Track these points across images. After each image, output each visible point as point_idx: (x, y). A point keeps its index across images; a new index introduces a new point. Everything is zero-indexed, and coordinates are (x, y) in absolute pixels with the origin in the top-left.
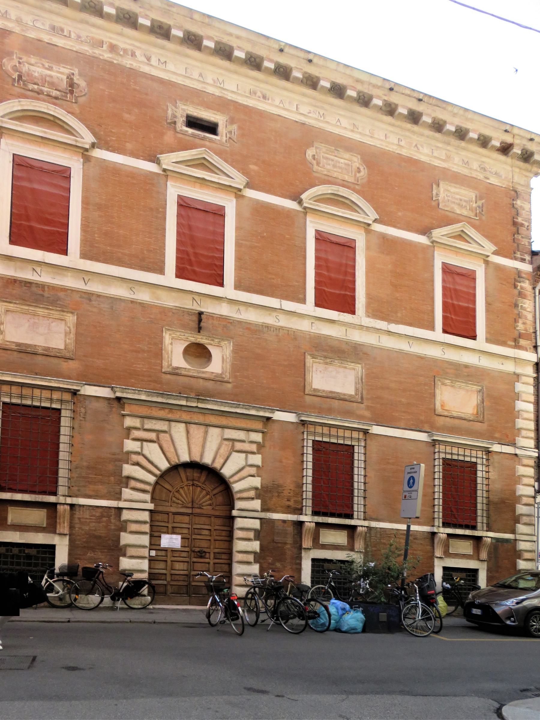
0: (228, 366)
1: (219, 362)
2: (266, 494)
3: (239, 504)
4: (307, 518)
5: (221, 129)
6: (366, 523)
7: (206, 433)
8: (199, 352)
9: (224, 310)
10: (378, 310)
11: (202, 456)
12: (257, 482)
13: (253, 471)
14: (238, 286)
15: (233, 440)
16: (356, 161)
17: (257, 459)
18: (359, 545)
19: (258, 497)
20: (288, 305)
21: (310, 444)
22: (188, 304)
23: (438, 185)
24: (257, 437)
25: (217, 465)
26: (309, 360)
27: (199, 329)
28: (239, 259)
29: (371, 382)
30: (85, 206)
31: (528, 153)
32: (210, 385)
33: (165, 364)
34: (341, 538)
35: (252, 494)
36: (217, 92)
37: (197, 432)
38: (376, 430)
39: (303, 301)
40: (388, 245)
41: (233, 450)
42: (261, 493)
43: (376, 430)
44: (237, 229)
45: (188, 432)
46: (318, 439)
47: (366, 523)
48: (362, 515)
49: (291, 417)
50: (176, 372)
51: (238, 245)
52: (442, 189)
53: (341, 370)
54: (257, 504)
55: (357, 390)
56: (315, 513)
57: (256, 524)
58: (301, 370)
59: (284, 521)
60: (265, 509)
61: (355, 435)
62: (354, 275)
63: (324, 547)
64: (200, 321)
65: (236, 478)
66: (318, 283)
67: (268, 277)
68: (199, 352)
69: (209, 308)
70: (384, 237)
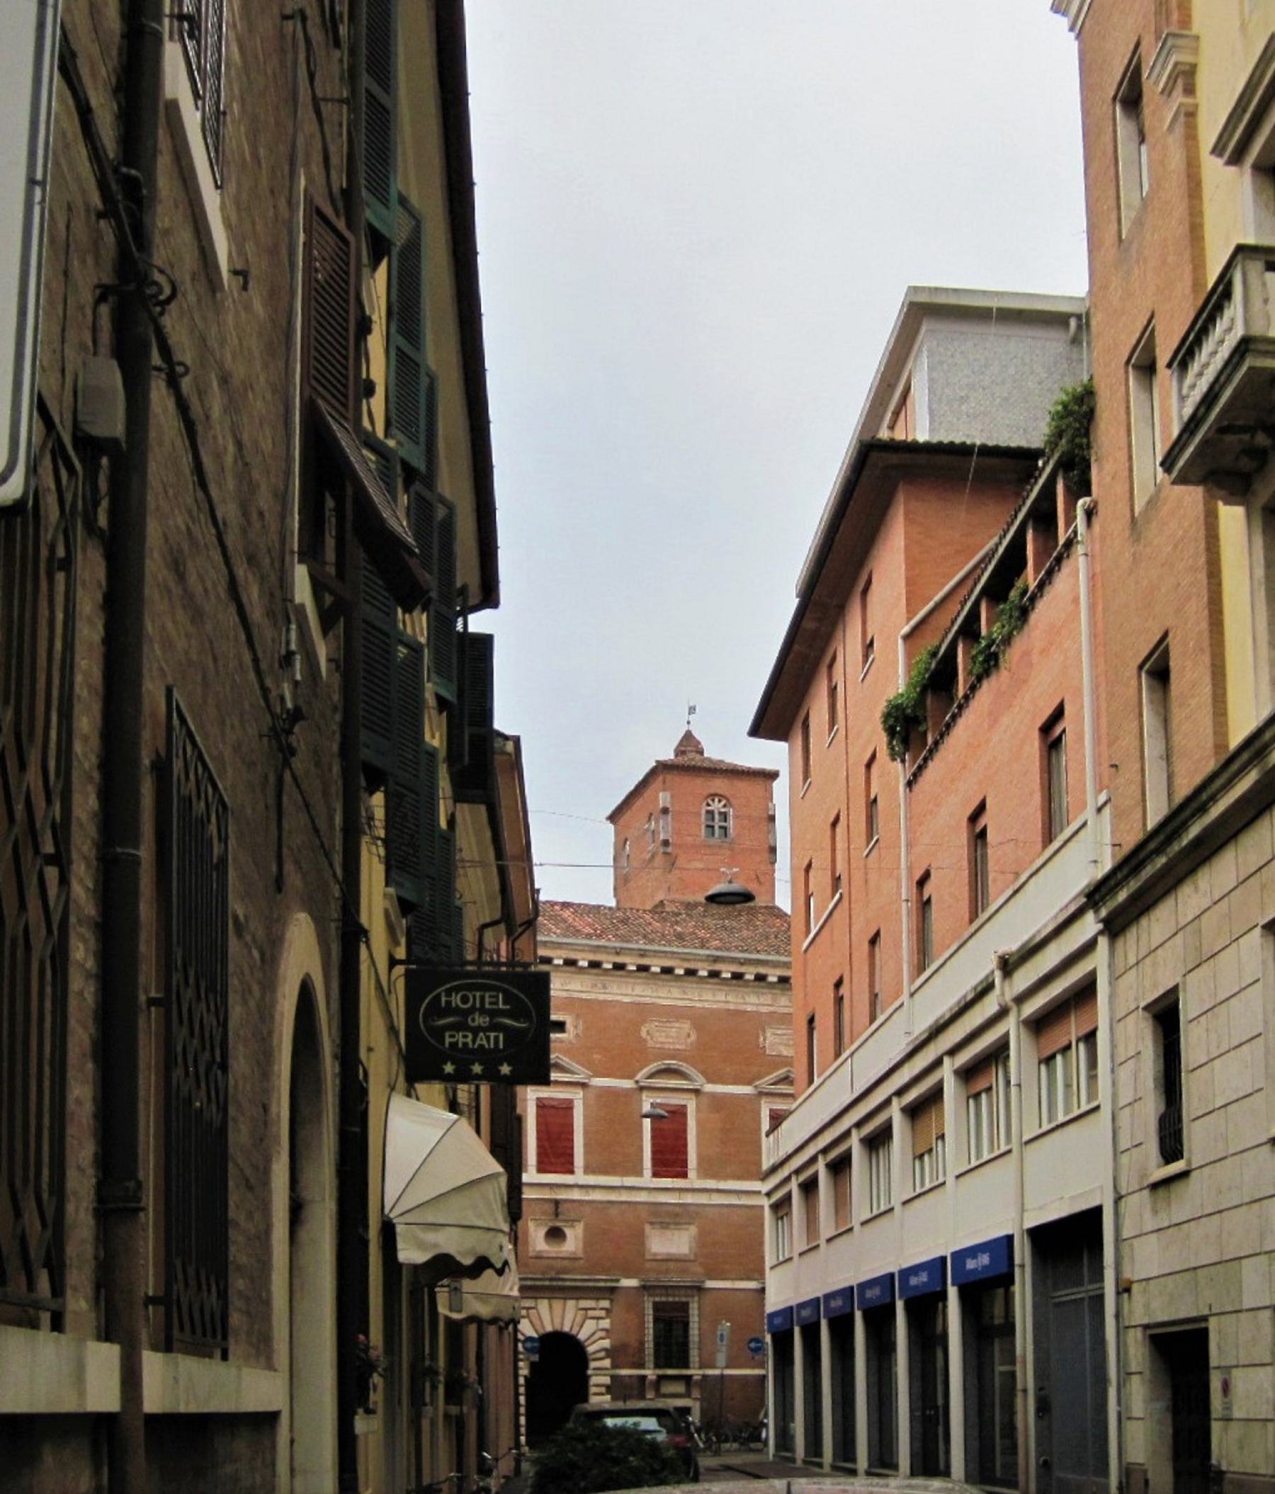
0: (581, 1245)
1: (573, 1242)
2: (616, 1354)
3: (593, 1364)
4: (650, 1373)
5: (569, 1026)
6: (701, 1372)
7: (565, 1305)
8: (555, 1234)
9: (576, 1195)
10: (707, 1170)
11: (562, 1324)
12: (606, 1343)
13: (603, 1334)
14: (588, 1170)
15: (586, 1309)
16: (686, 1026)
17: (606, 1323)
18: (696, 1393)
19: (607, 1356)
20: (630, 1181)
21: (651, 1305)
22: (547, 1195)
23: (764, 1031)
24: (605, 1304)
25: (574, 1332)
26: (648, 1228)
27: (557, 1215)
28: (587, 1145)
29: (703, 1241)
30: (1198, 220)
31: (218, 1353)
32: (566, 1263)
33: (531, 1249)
34: (680, 1388)
35: (602, 1354)
36: (565, 994)
37: (557, 1304)
38: (710, 1284)
39: (639, 1173)
40: (719, 1102)
41: (586, 1318)
42: (609, 1353)
43: (710, 1284)
44: (585, 1117)
45: (551, 1307)
46: (657, 1299)
47: (701, 1372)
48: (697, 1365)
49: (632, 1283)
50: (539, 1257)
51: (586, 1132)
52: (768, 1035)
53: (676, 1232)
54: (607, 1363)
55: (691, 1249)
56: (657, 1366)
57: (607, 1380)
58: (640, 1238)
59: (630, 1376)
60: (614, 1366)
61: (689, 1292)
62: (685, 1139)
63: (665, 1396)
64: (557, 1208)
65: (538, 1327)
66: (654, 1153)
67: (612, 1157)
68: (555, 1234)
69: (562, 1195)
70: (713, 1096)
